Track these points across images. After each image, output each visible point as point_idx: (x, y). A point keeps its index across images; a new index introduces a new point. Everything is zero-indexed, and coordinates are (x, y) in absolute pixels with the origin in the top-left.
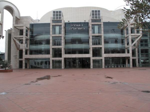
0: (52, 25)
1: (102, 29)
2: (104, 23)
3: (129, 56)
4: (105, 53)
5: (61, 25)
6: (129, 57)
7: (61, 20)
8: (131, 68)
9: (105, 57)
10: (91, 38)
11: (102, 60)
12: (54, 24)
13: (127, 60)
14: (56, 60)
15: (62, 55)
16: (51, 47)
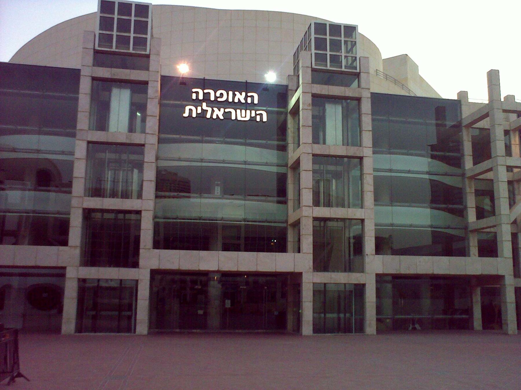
0: (94, 79)
1: (367, 121)
2: (376, 98)
3: (500, 273)
4: (157, 245)
5: (146, 83)
6: (499, 278)
7: (148, 56)
8: (69, 337)
9: (380, 272)
10: (306, 164)
11: (360, 289)
12: (104, 72)
13: (478, 291)
14: (103, 284)
15: (142, 252)
16: (75, 202)
